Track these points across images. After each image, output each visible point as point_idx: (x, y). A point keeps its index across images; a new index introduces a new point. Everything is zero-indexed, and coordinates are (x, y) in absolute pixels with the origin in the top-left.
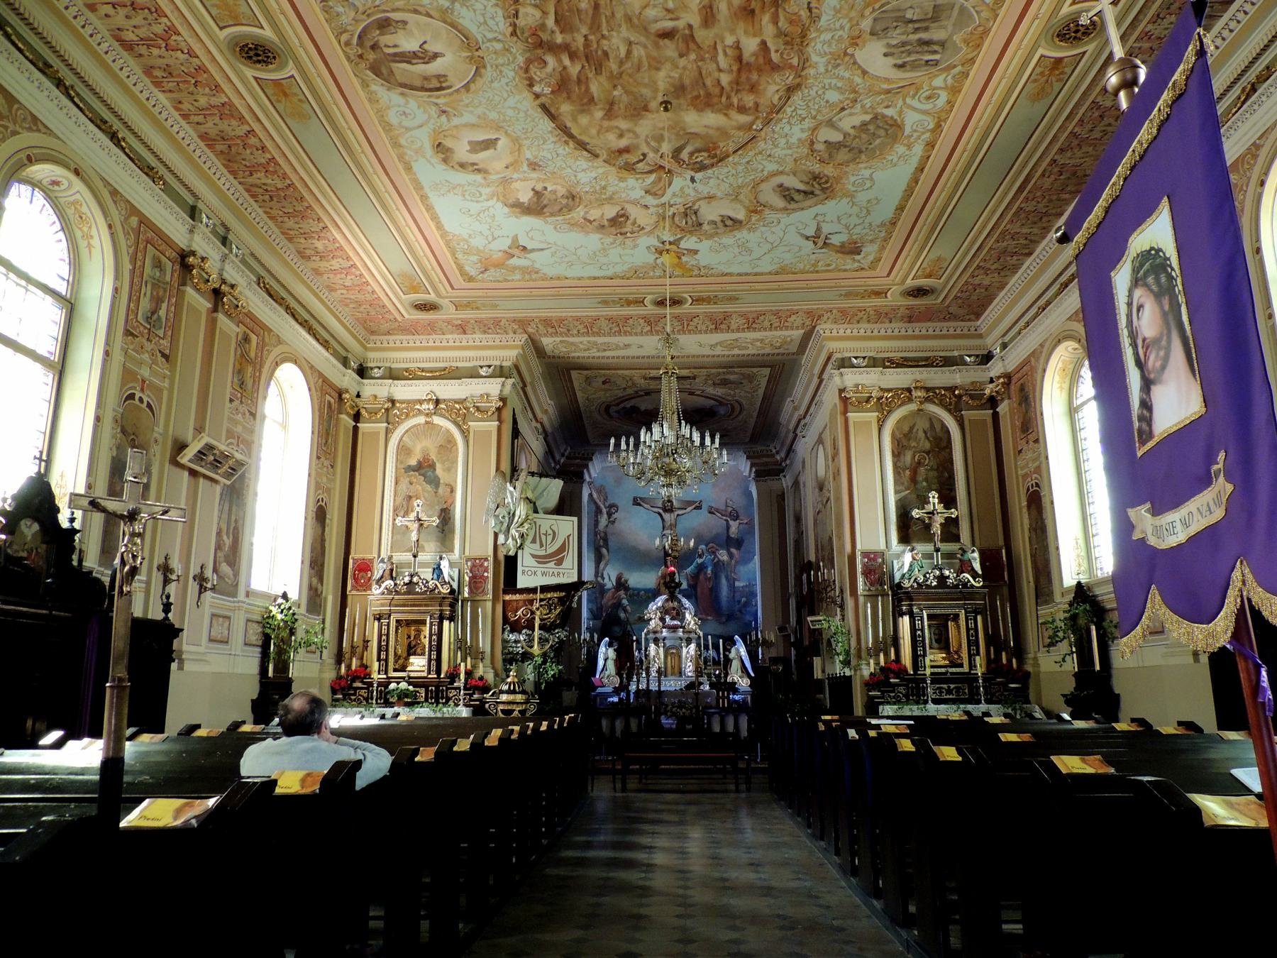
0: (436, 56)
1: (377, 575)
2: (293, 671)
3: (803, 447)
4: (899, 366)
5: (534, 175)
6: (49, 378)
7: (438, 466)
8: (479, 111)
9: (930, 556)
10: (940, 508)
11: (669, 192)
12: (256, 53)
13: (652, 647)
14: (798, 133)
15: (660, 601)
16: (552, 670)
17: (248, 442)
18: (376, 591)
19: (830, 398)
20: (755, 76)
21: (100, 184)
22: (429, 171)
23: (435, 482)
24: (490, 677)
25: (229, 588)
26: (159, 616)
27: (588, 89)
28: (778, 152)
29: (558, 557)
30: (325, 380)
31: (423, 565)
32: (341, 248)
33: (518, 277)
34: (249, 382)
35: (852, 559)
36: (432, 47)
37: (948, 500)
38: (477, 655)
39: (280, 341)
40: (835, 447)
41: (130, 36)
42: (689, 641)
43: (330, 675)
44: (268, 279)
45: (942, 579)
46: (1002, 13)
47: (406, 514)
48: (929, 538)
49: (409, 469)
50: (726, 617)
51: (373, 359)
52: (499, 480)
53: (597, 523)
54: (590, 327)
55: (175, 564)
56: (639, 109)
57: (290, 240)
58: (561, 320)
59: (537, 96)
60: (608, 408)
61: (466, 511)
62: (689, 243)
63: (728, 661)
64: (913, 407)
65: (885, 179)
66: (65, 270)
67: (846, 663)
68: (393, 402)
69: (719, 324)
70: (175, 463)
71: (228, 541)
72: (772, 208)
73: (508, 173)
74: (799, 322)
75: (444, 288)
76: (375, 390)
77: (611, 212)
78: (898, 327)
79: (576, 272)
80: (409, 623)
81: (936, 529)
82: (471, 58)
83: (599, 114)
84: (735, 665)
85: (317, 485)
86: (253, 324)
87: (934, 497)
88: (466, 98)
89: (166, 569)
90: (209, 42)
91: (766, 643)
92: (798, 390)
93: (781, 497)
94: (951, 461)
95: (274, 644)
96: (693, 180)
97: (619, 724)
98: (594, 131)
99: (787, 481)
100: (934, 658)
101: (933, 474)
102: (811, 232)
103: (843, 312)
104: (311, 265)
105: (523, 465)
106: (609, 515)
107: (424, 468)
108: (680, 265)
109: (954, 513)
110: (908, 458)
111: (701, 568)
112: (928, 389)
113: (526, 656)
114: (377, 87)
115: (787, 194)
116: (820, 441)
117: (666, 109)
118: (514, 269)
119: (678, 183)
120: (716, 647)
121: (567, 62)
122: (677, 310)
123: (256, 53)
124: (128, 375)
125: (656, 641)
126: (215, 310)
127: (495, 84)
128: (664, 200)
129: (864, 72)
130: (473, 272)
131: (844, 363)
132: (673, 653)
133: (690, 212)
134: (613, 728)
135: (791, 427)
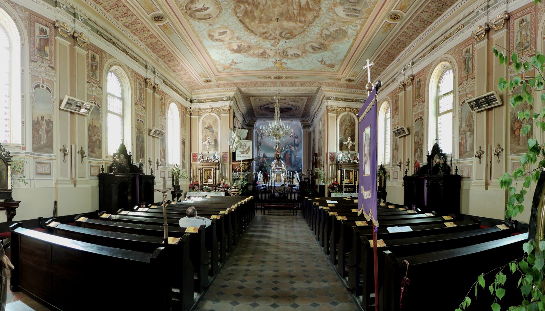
0: (208, 8)
1: (199, 158)
2: (180, 184)
3: (316, 120)
4: (343, 101)
5: (238, 41)
6: (121, 119)
7: (213, 127)
8: (221, 23)
9: (347, 154)
10: (351, 142)
11: (278, 46)
12: (158, 19)
13: (273, 174)
14: (317, 30)
15: (275, 161)
16: (245, 183)
17: (164, 126)
18: (199, 162)
19: (324, 108)
20: (305, 12)
21: (125, 67)
22: (207, 43)
23: (213, 132)
24: (229, 184)
25: (164, 165)
26: (150, 174)
27: (253, 15)
28: (311, 36)
29: (247, 152)
30: (182, 106)
31: (211, 155)
32: (184, 68)
33: (234, 71)
34: (164, 110)
35: (327, 154)
36: (206, 6)
37: (353, 140)
38: (226, 179)
39: (170, 97)
40: (324, 122)
41: (127, 24)
42: (283, 172)
43: (189, 184)
44: (166, 80)
45: (350, 161)
46: (376, 6)
47: (205, 141)
48: (347, 150)
49: (205, 128)
50: (294, 166)
51: (194, 97)
52: (230, 131)
53: (258, 139)
54: (255, 85)
55: (152, 160)
56: (269, 20)
57: (170, 68)
58: (247, 83)
59: (238, 17)
60: (261, 107)
61: (222, 140)
62: (284, 61)
63: (293, 178)
64: (346, 113)
65: (342, 47)
66: (120, 91)
67: (324, 182)
68: (200, 109)
69: (293, 84)
70: (149, 135)
71: (162, 153)
72: (309, 52)
73: (230, 41)
74: (316, 85)
75: (212, 76)
76: (195, 106)
77: (261, 51)
78: (344, 89)
79: (251, 69)
80: (207, 170)
81: (349, 147)
82: (218, 7)
83: (257, 22)
84: (295, 179)
85: (182, 135)
86: (163, 94)
87: (349, 139)
88: (217, 20)
89: (150, 162)
90: (146, 19)
91: (304, 175)
92: (315, 104)
93: (310, 133)
94: (355, 129)
95: (175, 178)
96: (285, 42)
97: (263, 196)
98: (256, 27)
99: (311, 129)
100: (346, 181)
101: (350, 132)
102: (320, 60)
103: (329, 83)
104: (176, 73)
105: (237, 126)
106: (261, 136)
107: (209, 128)
108: (282, 67)
109: (354, 143)
110: (343, 127)
111: (287, 152)
112: (350, 108)
113: (238, 179)
114: (191, 20)
115: (314, 48)
116: (321, 120)
117: (277, 21)
118: (233, 68)
119: (281, 43)
120: (290, 174)
121: (247, 6)
122: (280, 80)
123: (158, 19)
124: (137, 115)
125: (274, 172)
126: (154, 92)
127: (226, 15)
128: (277, 48)
129: (337, 15)
130: (221, 70)
131: (328, 99)
132: (278, 175)
133: (284, 52)
134: (262, 197)
135: (313, 114)
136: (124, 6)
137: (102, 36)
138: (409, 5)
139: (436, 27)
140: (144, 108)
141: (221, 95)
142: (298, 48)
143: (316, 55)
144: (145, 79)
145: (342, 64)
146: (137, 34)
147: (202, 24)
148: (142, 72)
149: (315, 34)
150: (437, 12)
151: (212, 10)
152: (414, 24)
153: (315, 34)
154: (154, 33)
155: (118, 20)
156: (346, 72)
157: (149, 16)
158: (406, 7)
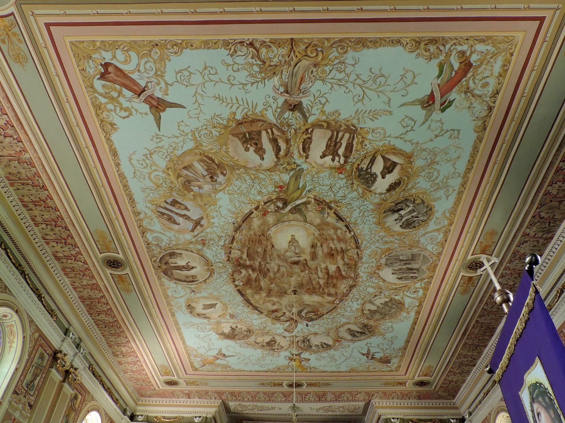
0: (193, 268)
5: (232, 321)
8: (209, 291)
11: (296, 331)
12: (114, 264)
14: (356, 306)
20: (335, 281)
21: (26, 317)
22: (183, 317)
27: (259, 284)
32: (134, 352)
33: (219, 369)
36: (191, 264)
39: (93, 399)
41: (60, 255)
44: (95, 366)
46: (442, 258)
54: (254, 397)
56: (282, 293)
57: (110, 346)
58: (240, 393)
59: (236, 286)
62: (305, 355)
65: (399, 327)
69: (321, 397)
72: (345, 339)
73: (220, 319)
75: (182, 373)
77: (268, 339)
83: (264, 295)
86: (82, 389)
88: (204, 286)
90: (94, 258)
96: (307, 325)
98: (261, 302)
102: (365, 352)
103: (384, 393)
104: (118, 359)
108: (301, 366)
114: (165, 280)
115: (353, 334)
117: (295, 294)
118: (219, 365)
119: (300, 326)
121: (251, 272)
122: (299, 390)
123: (114, 264)
126: (64, 381)
127: (218, 280)
128: (293, 334)
129: (384, 281)
130: (197, 366)
133: (306, 340)
136: (66, 228)
137: (7, 253)
138: (493, 243)
139: (552, 259)
140: (30, 406)
141: (190, 413)
142: (328, 335)
143: (357, 344)
144: (56, 352)
145: (402, 356)
146: (70, 275)
147: (180, 287)
148: (55, 337)
149: (352, 311)
150: (544, 236)
151: (199, 270)
152: (512, 266)
153: (352, 311)
154: (100, 283)
155: (47, 243)
156: (412, 369)
157: (100, 256)
158: (490, 246)
